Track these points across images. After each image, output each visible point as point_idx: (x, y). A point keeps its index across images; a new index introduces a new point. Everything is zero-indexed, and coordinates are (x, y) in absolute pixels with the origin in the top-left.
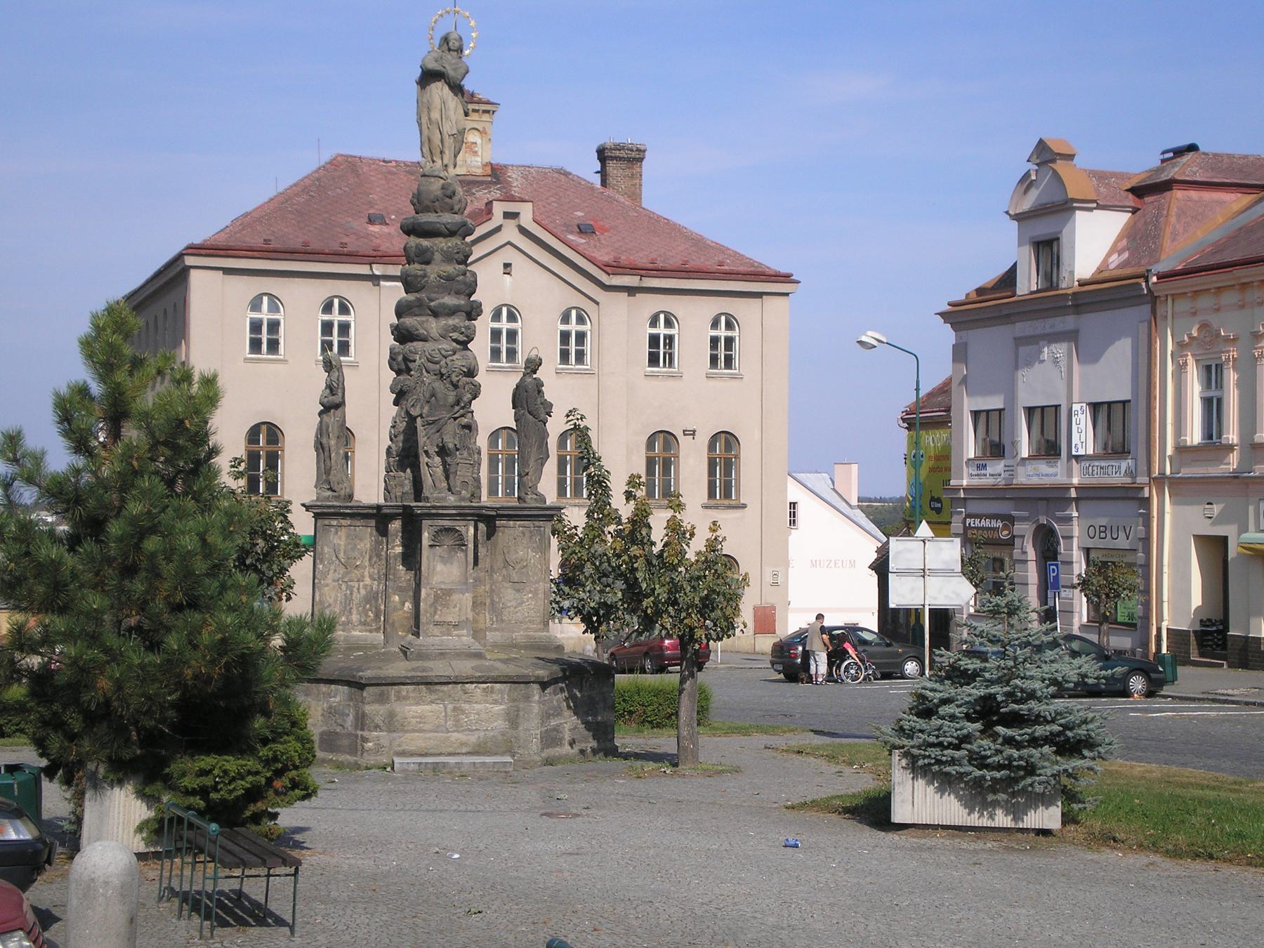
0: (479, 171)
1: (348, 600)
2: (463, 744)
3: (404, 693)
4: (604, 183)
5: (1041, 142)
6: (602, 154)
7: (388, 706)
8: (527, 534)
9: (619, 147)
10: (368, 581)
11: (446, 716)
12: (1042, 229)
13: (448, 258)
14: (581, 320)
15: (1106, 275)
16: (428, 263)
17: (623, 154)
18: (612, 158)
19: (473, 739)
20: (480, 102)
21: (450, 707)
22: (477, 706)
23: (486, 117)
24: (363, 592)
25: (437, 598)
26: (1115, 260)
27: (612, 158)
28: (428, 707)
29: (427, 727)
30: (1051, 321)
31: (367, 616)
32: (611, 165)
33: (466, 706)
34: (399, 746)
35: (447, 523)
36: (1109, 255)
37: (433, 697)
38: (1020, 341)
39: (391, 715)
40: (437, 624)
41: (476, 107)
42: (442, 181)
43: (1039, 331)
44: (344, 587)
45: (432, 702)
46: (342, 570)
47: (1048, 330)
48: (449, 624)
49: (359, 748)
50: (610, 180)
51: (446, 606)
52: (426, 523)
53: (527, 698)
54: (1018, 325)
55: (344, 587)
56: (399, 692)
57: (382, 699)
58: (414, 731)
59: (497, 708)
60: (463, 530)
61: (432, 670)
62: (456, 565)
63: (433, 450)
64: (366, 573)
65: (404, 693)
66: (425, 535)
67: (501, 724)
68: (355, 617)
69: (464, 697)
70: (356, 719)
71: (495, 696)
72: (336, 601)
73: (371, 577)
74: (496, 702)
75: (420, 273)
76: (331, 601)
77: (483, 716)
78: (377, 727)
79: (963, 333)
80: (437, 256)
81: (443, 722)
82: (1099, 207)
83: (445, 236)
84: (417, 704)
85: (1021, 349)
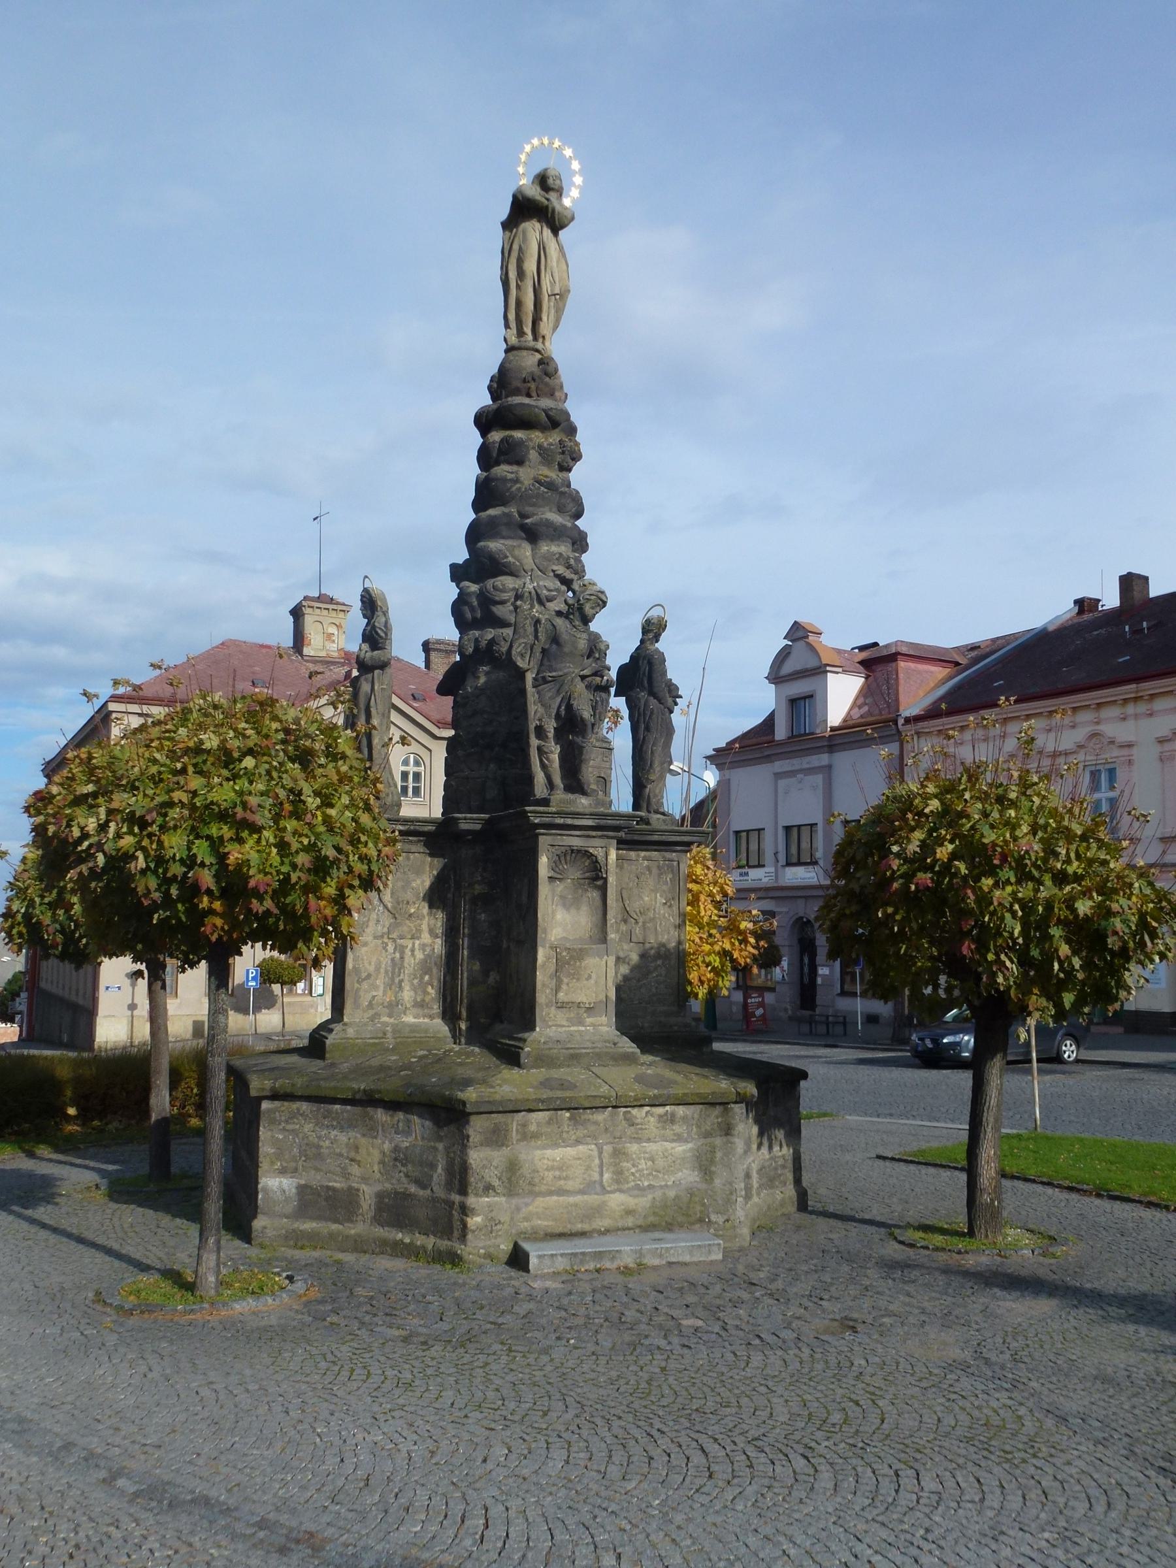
0: (336, 654)
1: (397, 966)
2: (629, 1212)
3: (533, 1128)
4: (428, 666)
5: (796, 622)
6: (427, 647)
7: (505, 1151)
8: (655, 871)
9: (439, 642)
10: (426, 938)
11: (601, 1166)
12: (798, 688)
13: (545, 455)
14: (417, 763)
15: (850, 723)
16: (520, 463)
17: (442, 647)
18: (435, 650)
19: (643, 1202)
20: (338, 603)
21: (608, 1149)
22: (652, 1147)
23: (341, 615)
24: (419, 955)
25: (560, 964)
26: (856, 714)
27: (435, 650)
28: (570, 1152)
29: (570, 1185)
30: (808, 759)
31: (425, 993)
32: (433, 655)
33: (634, 1148)
34: (526, 1219)
35: (576, 842)
36: (851, 709)
37: (581, 1132)
38: (778, 776)
39: (513, 1167)
40: (561, 1006)
41: (335, 607)
42: (538, 356)
43: (797, 767)
44: (391, 948)
45: (578, 1142)
46: (387, 920)
47: (805, 766)
48: (579, 1005)
49: (457, 1224)
50: (433, 666)
51: (576, 976)
52: (544, 841)
53: (727, 1130)
54: (777, 763)
55: (391, 948)
56: (524, 1125)
57: (497, 1138)
58: (550, 1193)
59: (680, 1149)
60: (599, 853)
61: (573, 1086)
62: (584, 908)
63: (551, 726)
64: (425, 927)
65: (533, 1128)
66: (543, 861)
67: (689, 1176)
68: (407, 995)
69: (630, 1131)
70: (449, 1170)
71: (677, 1128)
72: (378, 969)
73: (431, 932)
74: (679, 1138)
75: (510, 476)
76: (371, 969)
77: (660, 1163)
78: (488, 1188)
79: (727, 772)
80: (533, 455)
81: (596, 1177)
82: (844, 672)
83: (543, 429)
84: (556, 1145)
85: (779, 781)
